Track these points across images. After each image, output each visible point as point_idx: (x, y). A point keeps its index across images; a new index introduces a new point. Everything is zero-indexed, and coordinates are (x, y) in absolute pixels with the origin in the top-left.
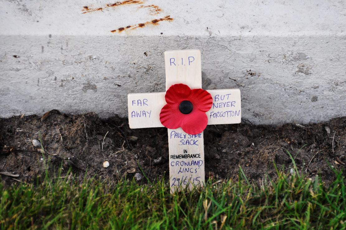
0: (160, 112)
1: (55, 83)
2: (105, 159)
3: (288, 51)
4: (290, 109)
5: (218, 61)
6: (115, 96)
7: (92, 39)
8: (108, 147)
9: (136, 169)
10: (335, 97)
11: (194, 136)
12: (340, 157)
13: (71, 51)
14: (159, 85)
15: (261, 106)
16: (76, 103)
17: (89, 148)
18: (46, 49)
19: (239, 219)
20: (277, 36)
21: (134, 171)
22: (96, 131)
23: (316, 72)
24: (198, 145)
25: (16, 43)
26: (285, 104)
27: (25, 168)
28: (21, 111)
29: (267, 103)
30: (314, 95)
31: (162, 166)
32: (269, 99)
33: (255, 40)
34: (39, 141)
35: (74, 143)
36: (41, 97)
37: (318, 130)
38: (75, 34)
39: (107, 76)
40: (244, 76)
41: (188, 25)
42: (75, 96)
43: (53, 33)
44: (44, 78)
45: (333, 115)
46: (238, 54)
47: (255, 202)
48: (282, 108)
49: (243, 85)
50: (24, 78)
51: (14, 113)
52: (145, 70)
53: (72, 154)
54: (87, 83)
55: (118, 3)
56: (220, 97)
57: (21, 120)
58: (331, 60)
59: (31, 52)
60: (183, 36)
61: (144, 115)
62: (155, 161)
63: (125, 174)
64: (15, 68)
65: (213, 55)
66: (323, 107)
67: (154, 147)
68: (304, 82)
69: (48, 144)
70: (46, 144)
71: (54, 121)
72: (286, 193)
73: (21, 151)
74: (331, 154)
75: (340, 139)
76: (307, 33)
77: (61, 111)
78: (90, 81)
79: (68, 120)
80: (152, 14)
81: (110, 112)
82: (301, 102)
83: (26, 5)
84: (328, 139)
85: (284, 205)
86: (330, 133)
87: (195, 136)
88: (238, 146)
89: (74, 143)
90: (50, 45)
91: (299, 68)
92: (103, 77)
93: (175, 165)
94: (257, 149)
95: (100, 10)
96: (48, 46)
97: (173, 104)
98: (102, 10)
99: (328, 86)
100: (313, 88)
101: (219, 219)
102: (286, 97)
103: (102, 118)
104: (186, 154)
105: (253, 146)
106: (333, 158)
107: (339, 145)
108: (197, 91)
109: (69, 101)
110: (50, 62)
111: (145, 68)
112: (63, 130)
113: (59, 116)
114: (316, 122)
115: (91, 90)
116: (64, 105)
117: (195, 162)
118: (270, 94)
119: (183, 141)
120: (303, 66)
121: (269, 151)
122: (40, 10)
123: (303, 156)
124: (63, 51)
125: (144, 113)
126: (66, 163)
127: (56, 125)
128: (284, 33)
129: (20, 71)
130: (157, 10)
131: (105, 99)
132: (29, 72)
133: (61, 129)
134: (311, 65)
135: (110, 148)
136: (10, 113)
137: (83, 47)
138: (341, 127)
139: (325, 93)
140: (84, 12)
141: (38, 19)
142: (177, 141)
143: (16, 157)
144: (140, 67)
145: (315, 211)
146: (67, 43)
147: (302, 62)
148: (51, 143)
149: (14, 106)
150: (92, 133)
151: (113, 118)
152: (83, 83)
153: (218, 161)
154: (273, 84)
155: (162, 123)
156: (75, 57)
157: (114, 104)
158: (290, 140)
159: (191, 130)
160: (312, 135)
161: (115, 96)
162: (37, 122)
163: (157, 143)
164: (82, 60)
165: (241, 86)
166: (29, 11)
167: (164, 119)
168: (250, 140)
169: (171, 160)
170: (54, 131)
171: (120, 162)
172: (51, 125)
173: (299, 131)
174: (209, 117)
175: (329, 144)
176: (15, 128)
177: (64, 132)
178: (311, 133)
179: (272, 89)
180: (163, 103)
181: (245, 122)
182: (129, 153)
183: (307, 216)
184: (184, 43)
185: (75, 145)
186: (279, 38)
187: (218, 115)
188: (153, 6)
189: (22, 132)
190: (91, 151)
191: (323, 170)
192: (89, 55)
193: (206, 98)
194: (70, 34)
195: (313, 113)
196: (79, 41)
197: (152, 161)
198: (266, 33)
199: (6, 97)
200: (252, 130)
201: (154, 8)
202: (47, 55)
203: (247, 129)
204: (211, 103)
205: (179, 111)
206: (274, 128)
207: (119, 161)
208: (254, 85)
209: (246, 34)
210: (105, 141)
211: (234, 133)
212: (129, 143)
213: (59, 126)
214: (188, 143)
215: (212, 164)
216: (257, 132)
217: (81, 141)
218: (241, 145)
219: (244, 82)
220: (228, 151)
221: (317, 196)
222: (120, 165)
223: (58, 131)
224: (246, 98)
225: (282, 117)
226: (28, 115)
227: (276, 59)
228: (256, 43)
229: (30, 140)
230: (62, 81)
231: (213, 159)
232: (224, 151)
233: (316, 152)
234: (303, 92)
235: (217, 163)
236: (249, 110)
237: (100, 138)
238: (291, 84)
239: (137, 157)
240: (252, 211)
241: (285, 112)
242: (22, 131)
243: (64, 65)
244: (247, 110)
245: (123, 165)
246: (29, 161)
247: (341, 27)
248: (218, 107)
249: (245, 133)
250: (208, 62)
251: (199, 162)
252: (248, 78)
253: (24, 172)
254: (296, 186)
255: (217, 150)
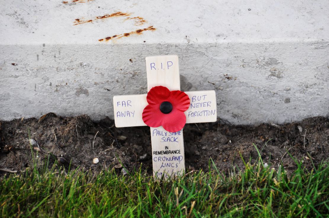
0: (142, 112)
1: (51, 88)
2: (96, 156)
3: (260, 56)
4: (265, 110)
5: (197, 66)
6: (105, 99)
7: (82, 47)
8: (98, 145)
9: (123, 164)
10: (306, 98)
11: (174, 134)
12: (311, 153)
13: (63, 59)
14: (144, 89)
15: (238, 107)
16: (71, 107)
17: (81, 147)
18: (41, 57)
19: (207, 205)
20: (249, 42)
21: (121, 166)
22: (87, 131)
23: (287, 76)
24: (178, 142)
25: (14, 52)
26: (261, 106)
27: (23, 165)
28: (21, 114)
29: (244, 105)
30: (287, 97)
31: (147, 162)
32: (246, 101)
33: (229, 46)
34: (36, 140)
35: (67, 142)
36: (38, 101)
37: (291, 129)
38: (66, 43)
39: (97, 81)
40: (222, 80)
41: (169, 34)
42: (69, 100)
43: (47, 43)
44: (41, 84)
45: (305, 115)
46: (214, 59)
47: (223, 190)
48: (258, 110)
49: (221, 88)
50: (22, 84)
51: (15, 116)
52: (131, 75)
53: (65, 151)
54: (79, 88)
55: (107, 15)
56: (196, 98)
57: (22, 123)
58: (300, 64)
59: (28, 60)
60: (164, 43)
61: (128, 115)
62: (141, 157)
63: (113, 169)
64: (14, 75)
65: (192, 60)
66: (295, 108)
67: (140, 145)
68: (277, 85)
69: (44, 143)
70: (41, 143)
71: (50, 123)
72: (252, 182)
73: (19, 149)
74: (302, 150)
75: (310, 136)
76: (277, 39)
77: (57, 114)
78: (82, 86)
79: (63, 121)
80: (137, 24)
81: (101, 114)
82: (275, 104)
83: (24, 18)
84: (300, 136)
85: (250, 192)
86: (302, 132)
87: (175, 134)
88: (217, 143)
89: (67, 142)
90: (44, 54)
91: (272, 72)
92: (93, 83)
93: (158, 160)
94: (234, 146)
95: (90, 22)
96: (42, 54)
97: (154, 104)
98: (92, 22)
99: (299, 88)
100: (284, 90)
101: (189, 205)
102: (261, 99)
103: (95, 120)
104: (167, 150)
105: (230, 143)
106: (304, 154)
107: (310, 142)
108: (175, 92)
109: (64, 104)
110: (45, 69)
111: (131, 74)
112: (58, 130)
113: (55, 118)
114: (290, 122)
115: (83, 94)
116: (60, 108)
117: (176, 157)
118: (247, 96)
119: (164, 138)
120: (275, 70)
121: (244, 148)
122: (36, 23)
123: (276, 152)
124: (56, 59)
125: (128, 113)
126: (59, 160)
127: (51, 126)
128: (256, 40)
129: (19, 78)
130: (141, 22)
131: (96, 103)
132: (26, 78)
133: (56, 130)
134: (282, 69)
135: (100, 146)
136: (11, 116)
137: (74, 55)
138: (312, 126)
139: (297, 95)
140: (75, 23)
141: (34, 30)
142: (159, 139)
143: (14, 155)
144: (127, 72)
145: (277, 197)
146: (60, 52)
147: (274, 67)
148: (47, 142)
149: (15, 110)
150: (83, 133)
151: (104, 119)
152: (75, 88)
153: (198, 157)
154: (249, 87)
155: (145, 122)
156: (67, 64)
157: (105, 108)
158: (264, 138)
159: (171, 128)
160: (285, 133)
161: (105, 99)
162: (35, 124)
163: (144, 142)
164: (73, 67)
165: (220, 89)
166: (26, 23)
167: (145, 119)
168: (228, 138)
169: (154, 156)
170: (49, 132)
171: (109, 159)
172: (47, 126)
173: (274, 130)
174: (187, 116)
175: (301, 141)
176: (15, 130)
177: (58, 132)
178: (284, 131)
179: (248, 92)
180: (145, 104)
181: (225, 123)
182: (118, 151)
183: (269, 203)
184: (164, 49)
185: (68, 144)
186: (251, 44)
187: (196, 114)
188: (138, 17)
189: (21, 133)
190: (82, 149)
191: (293, 164)
192: (80, 62)
193: (184, 98)
194: (62, 43)
195: (286, 114)
196: (70, 50)
197: (138, 158)
198: (240, 40)
199: (7, 101)
200: (231, 130)
201: (139, 20)
202: (42, 62)
203: (226, 129)
204: (189, 103)
205: (160, 111)
206: (251, 127)
207: (108, 158)
208: (231, 89)
209: (221, 41)
210: (96, 140)
211: (214, 132)
212: (118, 142)
213: (54, 127)
214: (168, 140)
215: (191, 158)
216: (236, 131)
217: (73, 140)
218: (220, 143)
219: (222, 85)
220: (207, 148)
221: (280, 184)
222: (109, 161)
223: (53, 131)
224: (224, 100)
225: (259, 118)
226: (27, 118)
227: (250, 64)
228: (230, 50)
229: (28, 140)
230: (57, 86)
231: (193, 155)
232: (204, 148)
233: (289, 148)
234: (277, 94)
235: (197, 159)
236: (228, 111)
237: (91, 137)
238: (264, 87)
239: (124, 154)
240: (219, 197)
241: (262, 113)
242: (21, 133)
243: (58, 71)
244: (227, 112)
245: (111, 162)
246: (26, 159)
247: (308, 34)
248: (196, 107)
249: (224, 132)
250: (188, 67)
251: (179, 157)
252: (225, 82)
253: (22, 168)
254: (261, 175)
255: (198, 147)
